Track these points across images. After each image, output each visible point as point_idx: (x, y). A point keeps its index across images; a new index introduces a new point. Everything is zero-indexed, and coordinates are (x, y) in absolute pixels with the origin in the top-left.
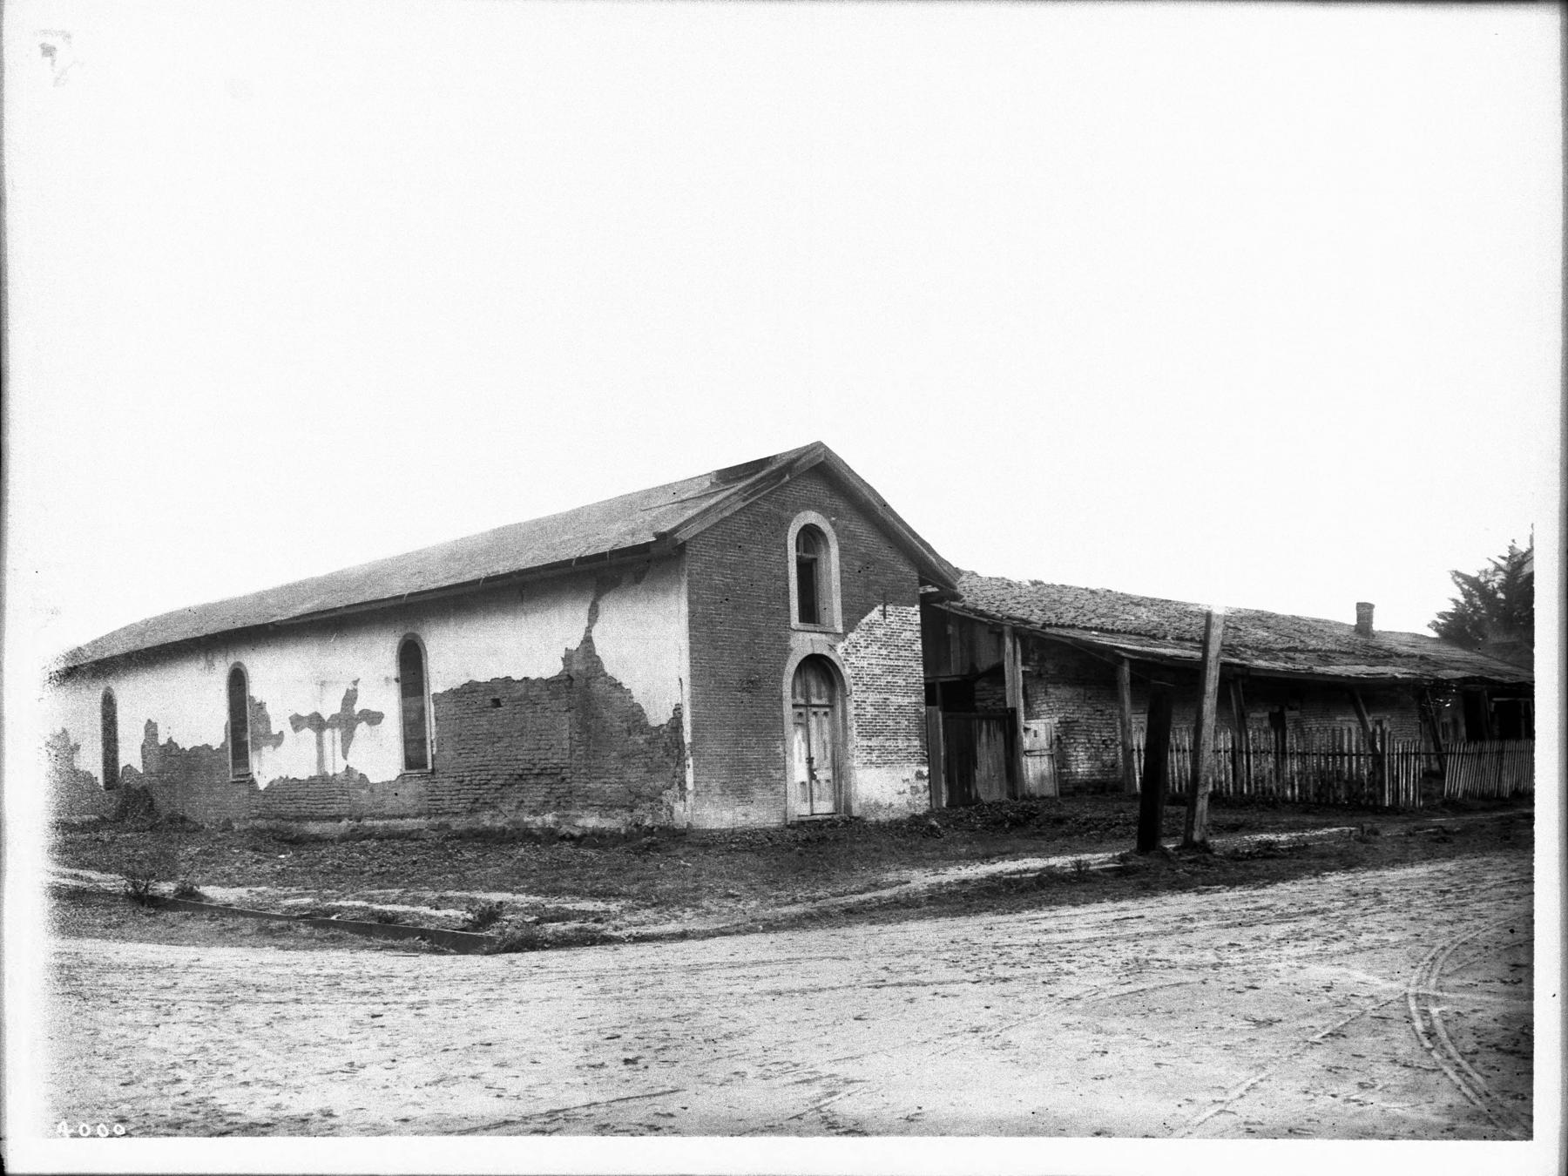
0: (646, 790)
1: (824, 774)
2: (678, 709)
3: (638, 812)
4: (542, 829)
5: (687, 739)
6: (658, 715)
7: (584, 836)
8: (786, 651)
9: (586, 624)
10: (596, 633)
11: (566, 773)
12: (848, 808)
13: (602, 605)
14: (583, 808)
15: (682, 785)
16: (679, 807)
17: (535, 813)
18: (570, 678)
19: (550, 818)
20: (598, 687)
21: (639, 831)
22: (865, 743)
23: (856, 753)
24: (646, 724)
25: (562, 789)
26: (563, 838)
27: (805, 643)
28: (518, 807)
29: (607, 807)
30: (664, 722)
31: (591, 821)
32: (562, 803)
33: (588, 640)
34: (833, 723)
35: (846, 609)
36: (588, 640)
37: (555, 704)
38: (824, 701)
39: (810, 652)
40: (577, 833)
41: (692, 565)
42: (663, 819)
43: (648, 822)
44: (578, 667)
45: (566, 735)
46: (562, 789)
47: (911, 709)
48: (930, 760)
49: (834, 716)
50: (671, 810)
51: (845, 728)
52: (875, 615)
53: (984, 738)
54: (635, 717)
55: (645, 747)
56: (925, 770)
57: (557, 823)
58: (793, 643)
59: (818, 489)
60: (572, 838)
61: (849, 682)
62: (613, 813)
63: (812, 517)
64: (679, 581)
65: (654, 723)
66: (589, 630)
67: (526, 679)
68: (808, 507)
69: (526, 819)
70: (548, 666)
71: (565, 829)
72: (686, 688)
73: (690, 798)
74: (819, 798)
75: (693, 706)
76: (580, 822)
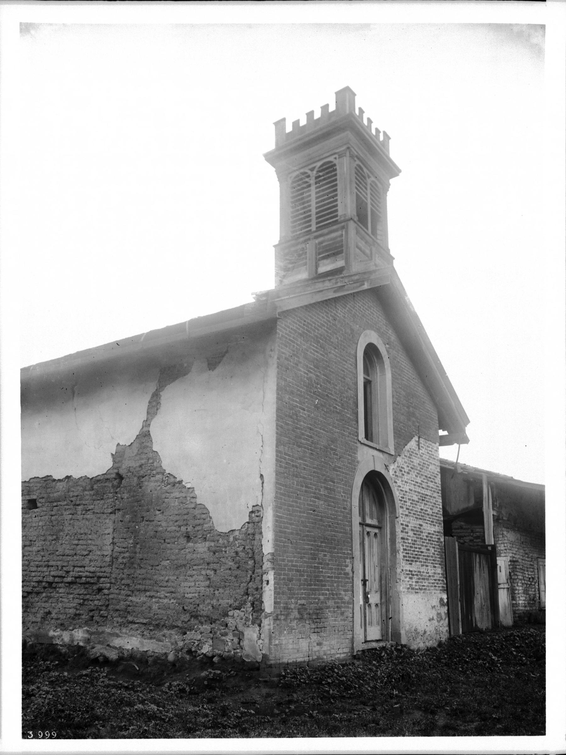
0: (205, 609)
1: (374, 598)
2: (256, 514)
3: (190, 635)
4: (69, 646)
5: (268, 548)
6: (228, 518)
7: (121, 659)
8: (353, 464)
9: (144, 417)
10: (154, 430)
11: (104, 583)
12: (396, 635)
13: (165, 395)
14: (121, 625)
15: (257, 607)
16: (251, 633)
17: (63, 626)
18: (120, 477)
19: (80, 635)
20: (151, 486)
21: (191, 660)
22: (408, 567)
23: (402, 578)
24: (211, 530)
25: (97, 601)
26: (95, 661)
27: (368, 460)
28: (44, 618)
29: (154, 626)
30: (237, 526)
31: (131, 642)
32: (94, 617)
33: (145, 436)
34: (382, 543)
35: (398, 433)
36: (145, 436)
37: (98, 506)
38: (374, 522)
39: (372, 469)
40: (113, 655)
41: (276, 350)
42: (229, 645)
43: (206, 649)
44: (127, 464)
45: (108, 540)
46: (97, 601)
47: (435, 538)
48: (447, 590)
49: (383, 536)
50: (240, 636)
51: (394, 551)
52: (412, 444)
53: (478, 569)
54: (195, 522)
55: (208, 557)
56: (445, 596)
57: (88, 641)
58: (359, 457)
59: (375, 313)
60: (106, 661)
61: (398, 504)
62: (159, 634)
63: (372, 337)
64: (266, 364)
65: (222, 528)
66: (147, 424)
67: (68, 477)
68: (371, 327)
69: (51, 633)
70: (94, 462)
71: (98, 650)
72: (270, 487)
73: (267, 623)
74: (371, 624)
75: (277, 508)
76: (117, 642)
